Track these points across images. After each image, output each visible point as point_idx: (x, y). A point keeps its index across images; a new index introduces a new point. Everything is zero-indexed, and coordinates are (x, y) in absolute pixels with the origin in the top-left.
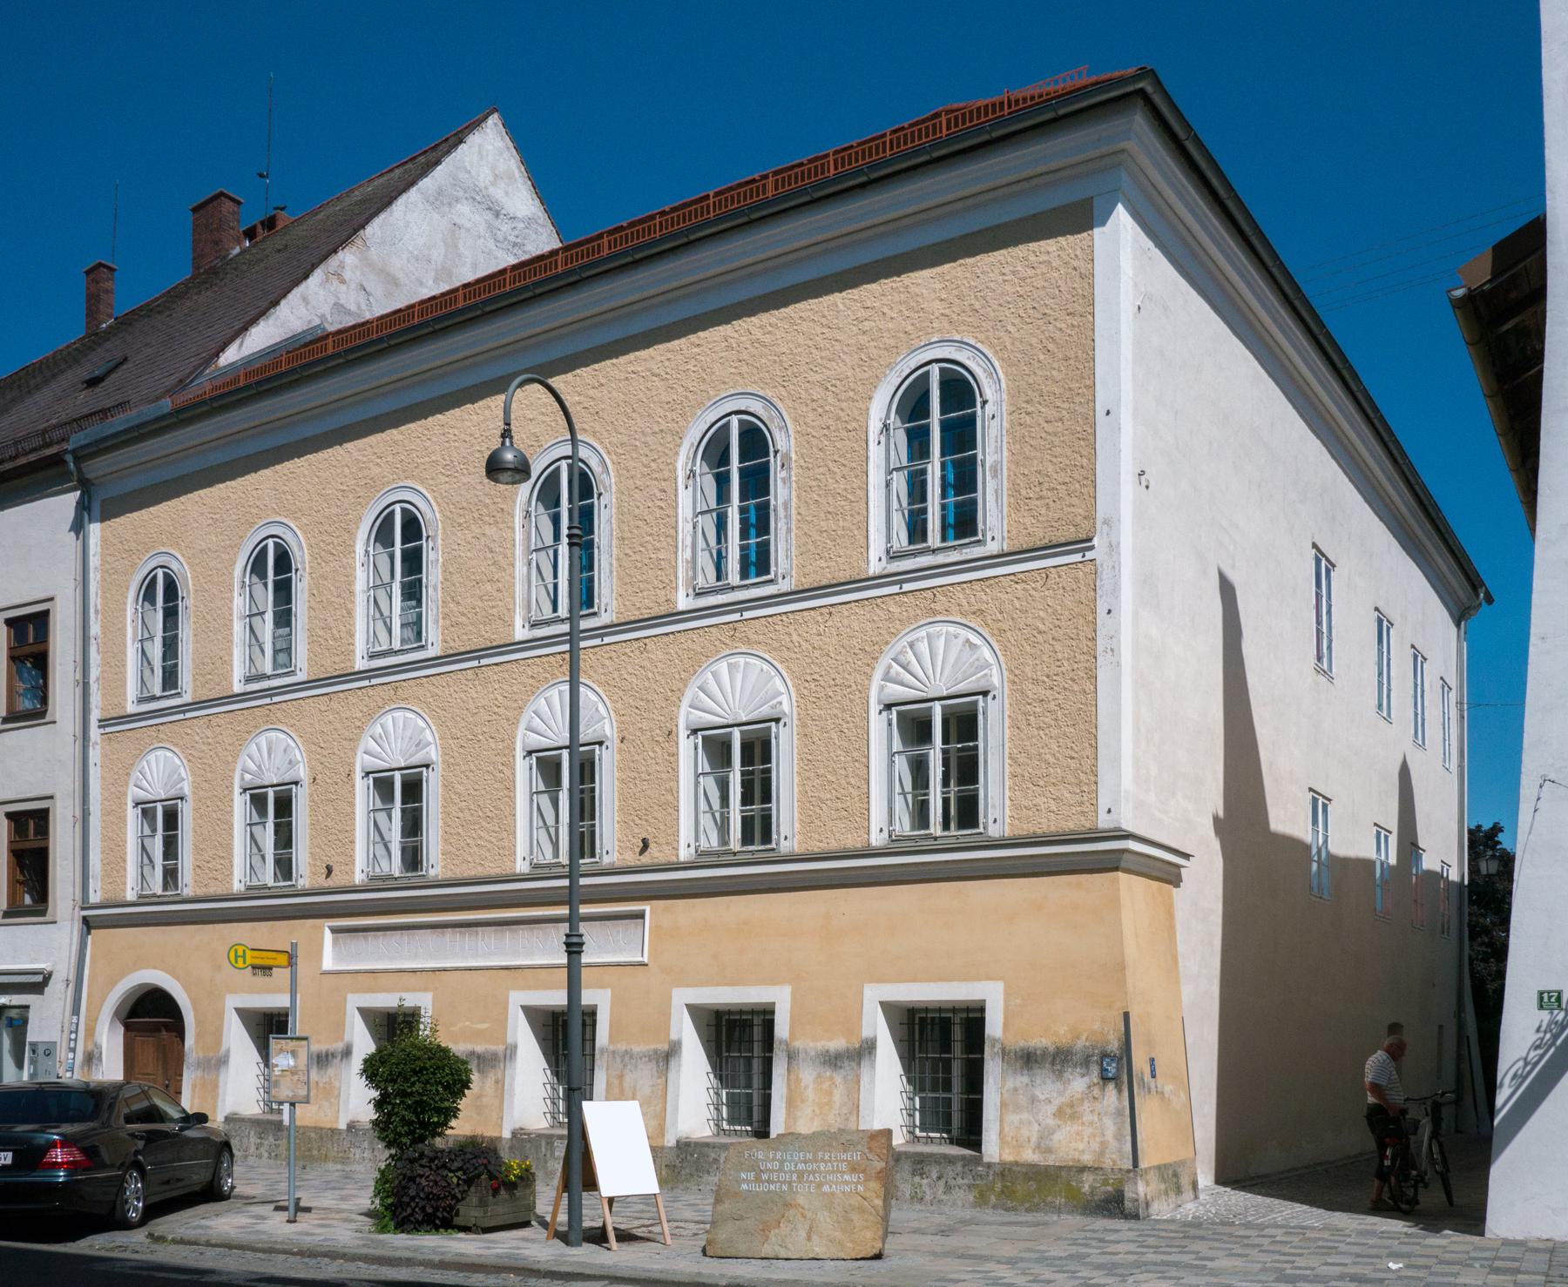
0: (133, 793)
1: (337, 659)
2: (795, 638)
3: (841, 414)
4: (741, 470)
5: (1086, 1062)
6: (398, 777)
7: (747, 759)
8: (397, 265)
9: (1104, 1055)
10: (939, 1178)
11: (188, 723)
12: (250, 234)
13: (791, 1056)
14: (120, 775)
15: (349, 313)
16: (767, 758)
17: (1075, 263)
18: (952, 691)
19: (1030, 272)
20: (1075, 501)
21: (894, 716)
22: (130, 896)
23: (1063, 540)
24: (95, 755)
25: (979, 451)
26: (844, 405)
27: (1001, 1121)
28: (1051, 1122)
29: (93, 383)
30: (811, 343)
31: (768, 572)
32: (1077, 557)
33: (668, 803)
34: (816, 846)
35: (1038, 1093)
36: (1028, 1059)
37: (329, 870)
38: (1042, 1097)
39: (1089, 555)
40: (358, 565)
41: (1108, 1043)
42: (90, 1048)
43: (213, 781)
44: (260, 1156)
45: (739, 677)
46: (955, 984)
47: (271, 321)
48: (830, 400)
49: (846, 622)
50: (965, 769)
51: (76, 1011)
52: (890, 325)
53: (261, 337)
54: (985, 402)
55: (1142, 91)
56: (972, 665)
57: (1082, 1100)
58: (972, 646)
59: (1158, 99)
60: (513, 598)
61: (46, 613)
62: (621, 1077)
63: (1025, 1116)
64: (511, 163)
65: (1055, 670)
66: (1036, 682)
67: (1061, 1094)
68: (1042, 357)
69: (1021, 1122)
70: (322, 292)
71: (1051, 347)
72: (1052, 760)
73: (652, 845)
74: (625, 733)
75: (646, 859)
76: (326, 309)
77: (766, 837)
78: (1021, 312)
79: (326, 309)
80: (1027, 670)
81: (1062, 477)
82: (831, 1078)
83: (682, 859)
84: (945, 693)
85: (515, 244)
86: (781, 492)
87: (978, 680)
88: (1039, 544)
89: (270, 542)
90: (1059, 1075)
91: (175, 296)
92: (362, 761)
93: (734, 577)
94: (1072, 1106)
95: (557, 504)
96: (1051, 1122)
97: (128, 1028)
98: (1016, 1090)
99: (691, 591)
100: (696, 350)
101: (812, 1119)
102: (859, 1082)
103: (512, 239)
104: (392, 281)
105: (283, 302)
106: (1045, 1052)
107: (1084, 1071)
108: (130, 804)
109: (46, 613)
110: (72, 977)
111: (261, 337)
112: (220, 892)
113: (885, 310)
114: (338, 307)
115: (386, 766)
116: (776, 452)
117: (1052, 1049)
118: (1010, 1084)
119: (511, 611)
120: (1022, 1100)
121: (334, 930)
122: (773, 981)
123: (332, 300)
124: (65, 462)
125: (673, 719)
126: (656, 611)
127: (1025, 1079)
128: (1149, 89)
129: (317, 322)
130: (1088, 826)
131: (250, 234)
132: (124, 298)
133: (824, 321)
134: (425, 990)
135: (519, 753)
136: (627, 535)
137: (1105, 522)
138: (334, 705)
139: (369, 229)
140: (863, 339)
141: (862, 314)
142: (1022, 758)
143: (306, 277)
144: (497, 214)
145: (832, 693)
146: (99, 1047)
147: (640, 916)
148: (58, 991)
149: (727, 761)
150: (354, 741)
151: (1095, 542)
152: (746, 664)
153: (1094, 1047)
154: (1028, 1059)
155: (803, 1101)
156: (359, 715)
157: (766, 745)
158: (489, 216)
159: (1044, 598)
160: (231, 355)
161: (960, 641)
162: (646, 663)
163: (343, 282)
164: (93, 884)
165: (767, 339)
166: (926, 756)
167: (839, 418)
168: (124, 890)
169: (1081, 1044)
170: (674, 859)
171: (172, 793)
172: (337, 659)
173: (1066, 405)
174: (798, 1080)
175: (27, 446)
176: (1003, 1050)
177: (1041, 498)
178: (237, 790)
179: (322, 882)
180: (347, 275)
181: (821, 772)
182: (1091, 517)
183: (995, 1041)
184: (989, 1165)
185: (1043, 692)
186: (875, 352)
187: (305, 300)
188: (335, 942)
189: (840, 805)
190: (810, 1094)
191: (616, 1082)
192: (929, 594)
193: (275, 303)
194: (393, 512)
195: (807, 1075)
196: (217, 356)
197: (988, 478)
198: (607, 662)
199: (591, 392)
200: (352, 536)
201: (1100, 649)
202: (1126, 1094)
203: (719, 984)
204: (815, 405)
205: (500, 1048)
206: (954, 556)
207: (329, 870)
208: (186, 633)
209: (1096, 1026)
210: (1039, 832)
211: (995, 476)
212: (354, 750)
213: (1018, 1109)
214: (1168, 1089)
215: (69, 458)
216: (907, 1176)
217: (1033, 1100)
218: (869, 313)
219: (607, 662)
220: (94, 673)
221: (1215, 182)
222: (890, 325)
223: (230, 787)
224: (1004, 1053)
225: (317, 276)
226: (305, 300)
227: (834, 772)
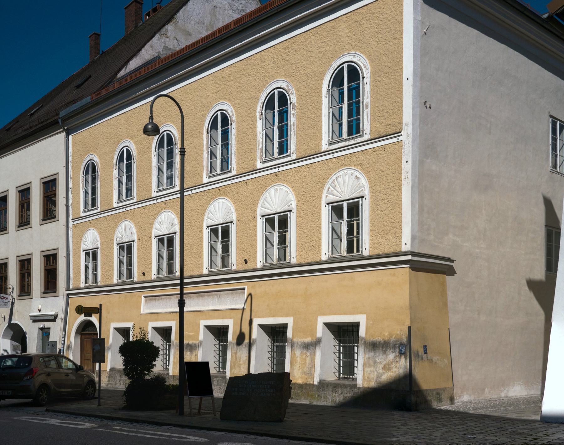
0: (83, 247)
1: (146, 193)
2: (297, 178)
3: (313, 86)
4: (278, 111)
5: (394, 347)
6: (345, 204)
7: (350, 215)
8: (191, 27)
9: (401, 344)
10: (341, 393)
11: (100, 219)
12: (148, 14)
13: (293, 345)
14: (79, 239)
15: (170, 49)
17: (396, 17)
18: (351, 197)
19: (380, 22)
20: (395, 117)
21: (330, 208)
22: (82, 286)
23: (391, 133)
24: (71, 233)
25: (361, 98)
26: (314, 82)
27: (364, 371)
28: (381, 371)
29: (78, 87)
30: (302, 58)
31: (360, 133)
32: (395, 140)
33: (253, 245)
34: (304, 261)
35: (377, 359)
36: (374, 346)
37: (144, 274)
38: (378, 361)
39: (400, 138)
40: (153, 156)
41: (402, 339)
42: (69, 343)
43: (145, 235)
44: (120, 384)
45: (278, 195)
46: (349, 315)
47: (138, 57)
48: (309, 81)
49: (314, 170)
51: (65, 330)
52: (330, 49)
53: (134, 64)
54: (363, 78)
56: (357, 186)
57: (392, 362)
58: (357, 177)
60: (203, 166)
61: (55, 179)
62: (236, 353)
63: (372, 369)
67: (385, 360)
68: (384, 57)
69: (370, 371)
70: (159, 43)
71: (387, 53)
72: (386, 224)
73: (248, 262)
74: (239, 218)
75: (246, 267)
78: (377, 39)
79: (160, 49)
80: (377, 187)
81: (391, 107)
82: (306, 353)
83: (204, 273)
84: (348, 198)
85: (241, 10)
86: (293, 120)
87: (360, 192)
88: (382, 135)
89: (125, 149)
90: (385, 353)
92: (260, 211)
93: (345, 135)
94: (389, 365)
95: (274, 109)
96: (381, 371)
97: (82, 335)
98: (369, 358)
99: (261, 161)
100: (264, 64)
101: (299, 370)
102: (315, 355)
104: (189, 34)
105: (143, 50)
106: (380, 342)
107: (393, 351)
108: (82, 251)
109: (55, 179)
110: (63, 317)
111: (134, 64)
112: (110, 283)
113: (328, 42)
114: (165, 48)
115: (271, 212)
116: (291, 103)
117: (382, 341)
118: (367, 356)
119: (202, 171)
120: (371, 362)
121: (145, 297)
122: (287, 315)
123: (163, 45)
124: (58, 122)
125: (255, 212)
127: (373, 354)
129: (156, 55)
130: (398, 250)
131: (148, 14)
132: (105, 46)
133: (307, 49)
134: (173, 320)
135: (205, 227)
136: (240, 140)
137: (406, 125)
138: (146, 211)
139: (178, 14)
140: (321, 55)
141: (321, 45)
142: (375, 223)
145: (308, 199)
146: (71, 343)
147: (244, 289)
148: (59, 321)
149: (341, 217)
150: (152, 224)
151: (402, 133)
152: (223, 202)
153: (397, 341)
154: (374, 346)
155: (296, 363)
156: (153, 214)
159: (384, 157)
160: (122, 73)
161: (354, 176)
162: (246, 190)
163: (167, 37)
164: (71, 282)
165: (288, 58)
167: (312, 88)
168: (80, 284)
169: (393, 339)
170: (255, 267)
171: (95, 247)
172: (146, 193)
173: (393, 77)
174: (295, 354)
176: (365, 342)
177: (383, 116)
178: (115, 244)
179: (142, 278)
180: (169, 34)
182: (401, 123)
183: (362, 338)
184: (359, 388)
186: (325, 60)
188: (146, 301)
189: (312, 244)
190: (299, 359)
191: (234, 355)
192: (342, 158)
193: (140, 50)
194: (217, 115)
195: (298, 352)
196: (117, 74)
197: (365, 109)
198: (234, 190)
199: (228, 84)
200: (151, 144)
201: (403, 178)
202: (408, 360)
203: (269, 317)
204: (303, 83)
205: (197, 342)
206: (352, 142)
207: (246, 262)
208: (99, 185)
209: (398, 332)
210: (381, 253)
211: (367, 108)
212: (152, 227)
213: (370, 366)
214: (435, 359)
215: (60, 120)
216: (330, 392)
217: (375, 362)
218: (323, 44)
219: (234, 190)
220: (71, 202)
222: (330, 49)
223: (113, 243)
224: (366, 343)
226: (152, 47)
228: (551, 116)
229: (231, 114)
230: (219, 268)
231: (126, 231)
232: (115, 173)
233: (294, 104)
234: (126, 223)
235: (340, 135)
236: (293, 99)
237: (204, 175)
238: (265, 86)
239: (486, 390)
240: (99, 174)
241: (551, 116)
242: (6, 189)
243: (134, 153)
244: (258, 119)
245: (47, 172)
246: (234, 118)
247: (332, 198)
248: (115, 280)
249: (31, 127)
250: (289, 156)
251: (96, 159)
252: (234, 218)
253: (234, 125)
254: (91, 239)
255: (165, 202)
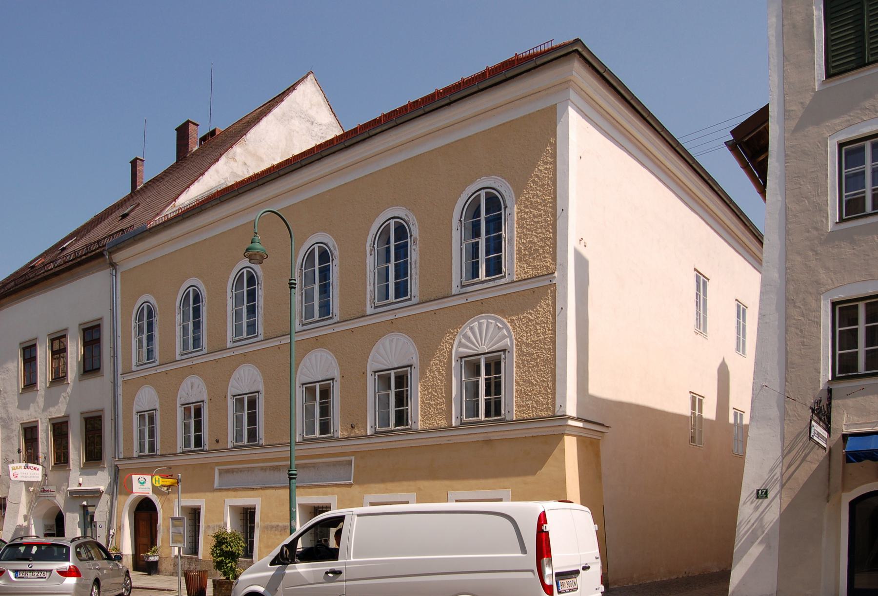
0: (136, 408)
14: (130, 399)
15: (238, 176)
16: (498, 371)
21: (463, 363)
22: (135, 455)
29: (124, 216)
37: (217, 441)
50: (494, 387)
54: (506, 207)
55: (576, 51)
59: (584, 53)
61: (99, 326)
64: (319, 98)
65: (536, 338)
66: (528, 345)
76: (227, 175)
77: (498, 412)
80: (524, 339)
91: (167, 173)
103: (320, 134)
109: (99, 326)
114: (234, 174)
126: (357, 315)
128: (580, 50)
132: (147, 174)
143: (218, 160)
144: (312, 123)
147: (349, 463)
151: (556, 274)
157: (498, 364)
158: (308, 124)
166: (478, 381)
175: (80, 253)
180: (237, 158)
181: (430, 391)
185: (530, 350)
187: (217, 172)
206: (491, 284)
207: (217, 441)
221: (623, 92)
225: (223, 160)
226: (217, 172)
227: (436, 392)
228: (695, 270)
229: (332, 249)
230: (147, 453)
231: (193, 389)
232: (179, 318)
233: (415, 238)
234: (193, 380)
235: (475, 274)
236: (415, 231)
237: (368, 306)
238: (472, 182)
239: (152, 559)
240: (157, 319)
241: (695, 270)
242: (64, 328)
243: (204, 294)
244: (368, 255)
245: (89, 316)
246: (336, 253)
247: (183, 401)
248: (230, 443)
249: (65, 263)
250: (410, 299)
251: (153, 300)
252: (336, 374)
253: (336, 262)
254: (147, 398)
255: (245, 354)
